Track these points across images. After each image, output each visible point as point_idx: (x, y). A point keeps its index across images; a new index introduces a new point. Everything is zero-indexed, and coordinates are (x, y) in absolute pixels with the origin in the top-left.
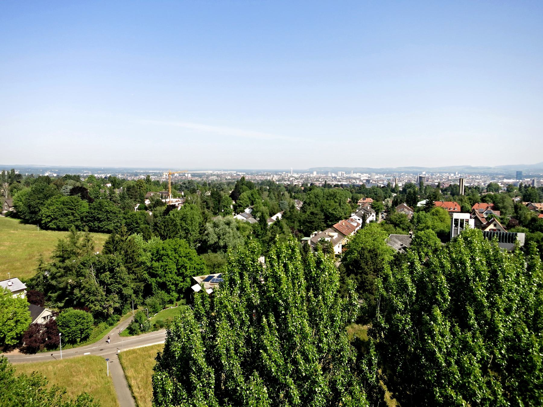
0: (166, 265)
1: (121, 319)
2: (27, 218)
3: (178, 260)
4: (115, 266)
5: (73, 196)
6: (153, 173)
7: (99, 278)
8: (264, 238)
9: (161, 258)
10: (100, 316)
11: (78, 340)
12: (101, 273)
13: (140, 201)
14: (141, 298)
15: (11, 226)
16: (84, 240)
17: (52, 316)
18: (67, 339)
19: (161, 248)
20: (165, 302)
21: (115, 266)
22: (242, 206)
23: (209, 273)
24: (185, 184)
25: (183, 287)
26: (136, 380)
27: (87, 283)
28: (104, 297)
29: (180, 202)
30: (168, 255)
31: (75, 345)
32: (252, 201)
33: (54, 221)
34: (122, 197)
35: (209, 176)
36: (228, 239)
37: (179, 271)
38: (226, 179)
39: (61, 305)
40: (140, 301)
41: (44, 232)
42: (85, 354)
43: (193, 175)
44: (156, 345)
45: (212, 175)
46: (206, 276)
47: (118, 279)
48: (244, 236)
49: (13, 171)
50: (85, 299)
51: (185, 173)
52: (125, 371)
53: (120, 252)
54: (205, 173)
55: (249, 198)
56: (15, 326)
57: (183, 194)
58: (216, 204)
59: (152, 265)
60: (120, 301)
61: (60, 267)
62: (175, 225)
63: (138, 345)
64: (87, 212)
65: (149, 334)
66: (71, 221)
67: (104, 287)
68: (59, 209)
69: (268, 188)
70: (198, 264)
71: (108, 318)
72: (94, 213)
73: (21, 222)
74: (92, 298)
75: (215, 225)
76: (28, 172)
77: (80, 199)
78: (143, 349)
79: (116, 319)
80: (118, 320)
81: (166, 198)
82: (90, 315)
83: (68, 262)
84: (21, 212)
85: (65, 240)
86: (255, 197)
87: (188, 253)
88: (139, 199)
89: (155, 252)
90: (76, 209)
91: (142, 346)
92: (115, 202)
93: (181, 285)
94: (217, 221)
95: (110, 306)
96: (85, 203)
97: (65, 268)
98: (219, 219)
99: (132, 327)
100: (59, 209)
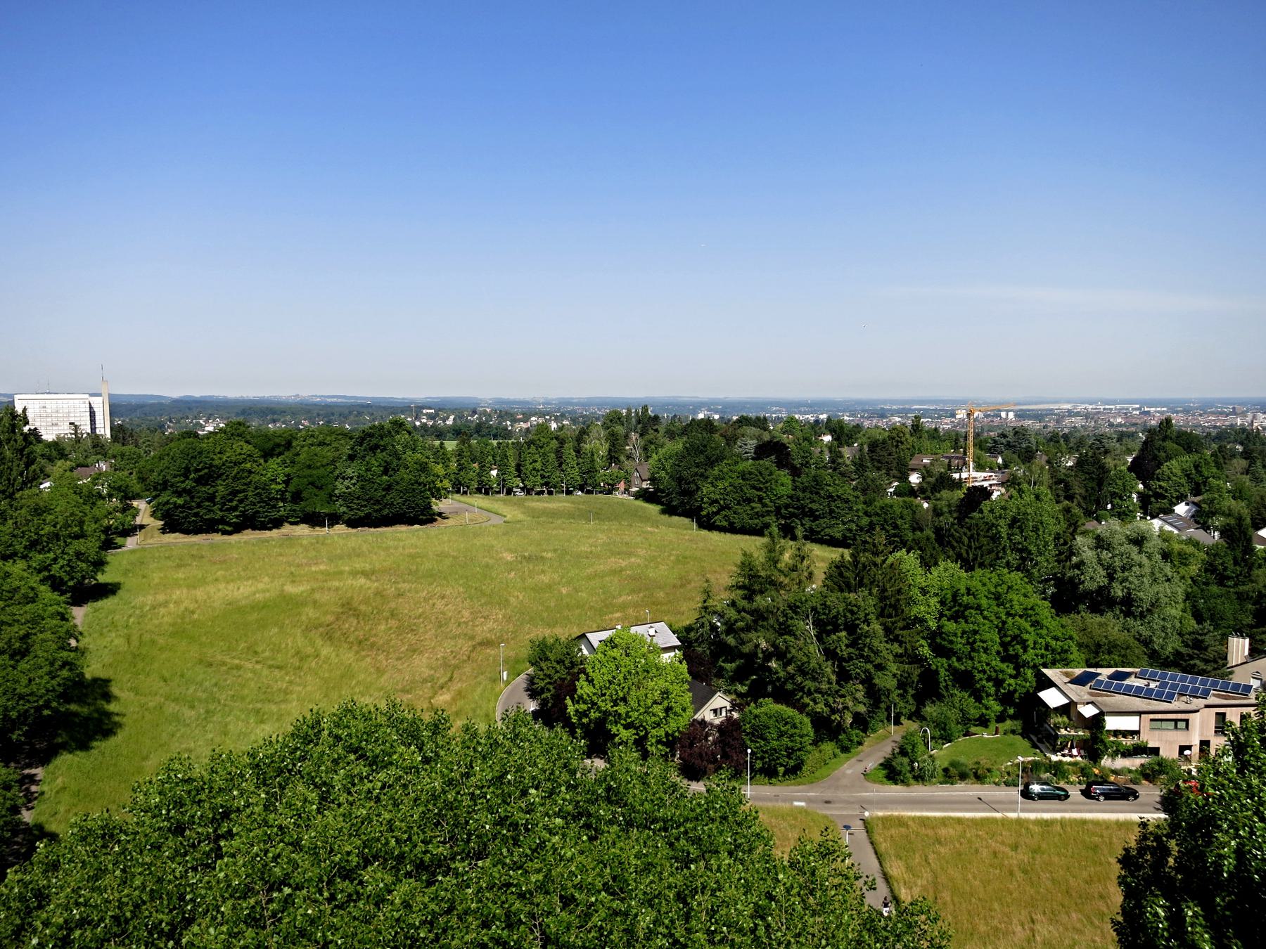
0: (975, 632)
1: (867, 742)
2: (675, 503)
3: (1004, 623)
4: (859, 619)
5: (761, 462)
6: (921, 410)
7: (824, 643)
8: (1241, 588)
9: (963, 612)
10: (826, 728)
11: (781, 770)
12: (828, 633)
13: (899, 475)
14: (911, 700)
15: (646, 519)
16: (793, 557)
17: (731, 711)
18: (759, 764)
19: (963, 591)
20: (970, 720)
21: (859, 619)
22: (1164, 497)
23: (1084, 664)
24: (1004, 436)
25: (1015, 691)
26: (911, 888)
27: (801, 649)
28: (836, 687)
29: (995, 482)
30: (979, 608)
31: (774, 780)
32: (1197, 484)
33: (724, 513)
34: (860, 466)
35: (1063, 417)
36: (1136, 582)
37: (1006, 650)
38: (1111, 425)
39: (743, 689)
40: (909, 707)
41: (704, 533)
42: (796, 803)
43: (1020, 415)
44: (952, 818)
45: (1070, 413)
46: (1078, 671)
47: (866, 649)
48: (1183, 578)
49: (645, 408)
50: (795, 684)
51: (1000, 411)
52: (884, 864)
53: (870, 590)
54: (1052, 410)
55: (1188, 476)
56: (664, 718)
57: (1000, 460)
58: (1092, 488)
59: (939, 627)
60: (865, 700)
61: (744, 610)
62: (995, 539)
63: (912, 810)
64: (788, 497)
65: (934, 788)
66: (757, 513)
67: (833, 665)
68: (735, 487)
69: (1239, 448)
70: (1056, 639)
71: (840, 734)
72: (803, 500)
73: (663, 512)
74: (809, 684)
75: (1101, 543)
76: (667, 411)
77: (774, 468)
78: (923, 822)
79: (856, 739)
80: (860, 743)
81: (959, 470)
82: (807, 720)
83: (762, 602)
84: (663, 491)
85: (755, 555)
86: (1206, 474)
87: (1032, 609)
88: (895, 472)
89: (949, 596)
90: (766, 488)
91: (918, 814)
92: (842, 474)
93: (1009, 685)
94: (1108, 534)
95: (846, 708)
96: (784, 477)
97: (751, 613)
98: (1110, 526)
99: (894, 763)
100: (735, 487)
